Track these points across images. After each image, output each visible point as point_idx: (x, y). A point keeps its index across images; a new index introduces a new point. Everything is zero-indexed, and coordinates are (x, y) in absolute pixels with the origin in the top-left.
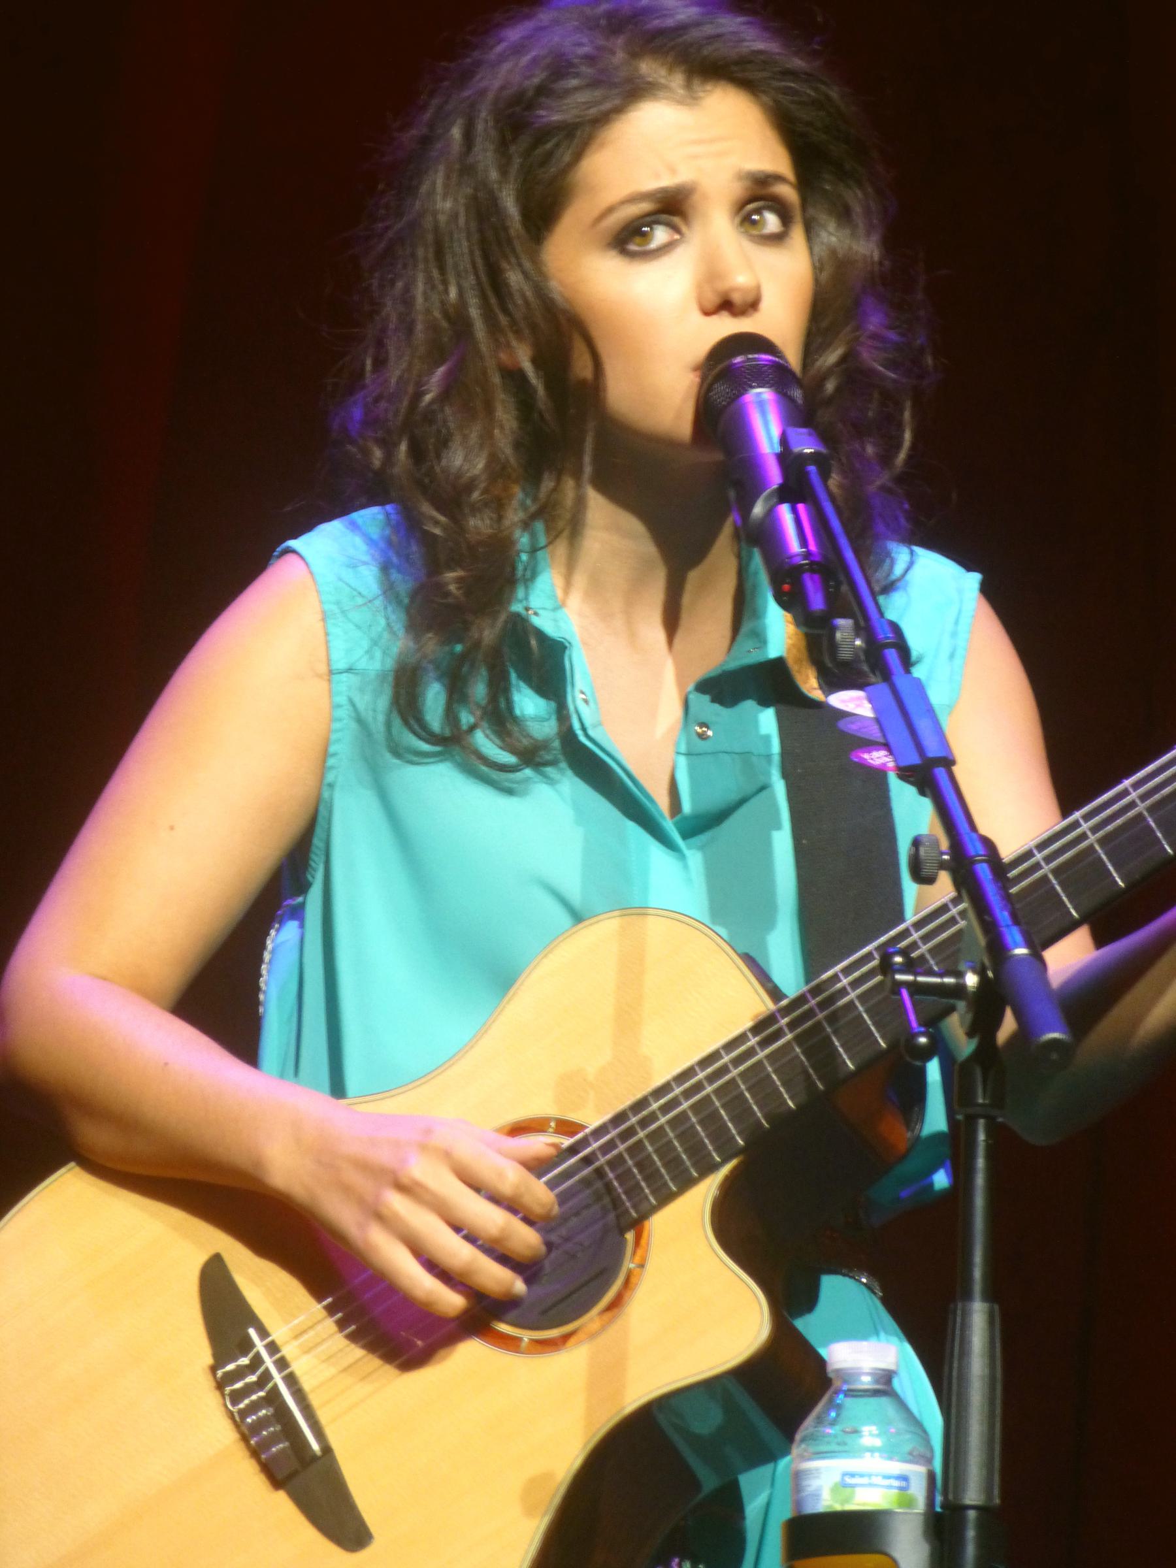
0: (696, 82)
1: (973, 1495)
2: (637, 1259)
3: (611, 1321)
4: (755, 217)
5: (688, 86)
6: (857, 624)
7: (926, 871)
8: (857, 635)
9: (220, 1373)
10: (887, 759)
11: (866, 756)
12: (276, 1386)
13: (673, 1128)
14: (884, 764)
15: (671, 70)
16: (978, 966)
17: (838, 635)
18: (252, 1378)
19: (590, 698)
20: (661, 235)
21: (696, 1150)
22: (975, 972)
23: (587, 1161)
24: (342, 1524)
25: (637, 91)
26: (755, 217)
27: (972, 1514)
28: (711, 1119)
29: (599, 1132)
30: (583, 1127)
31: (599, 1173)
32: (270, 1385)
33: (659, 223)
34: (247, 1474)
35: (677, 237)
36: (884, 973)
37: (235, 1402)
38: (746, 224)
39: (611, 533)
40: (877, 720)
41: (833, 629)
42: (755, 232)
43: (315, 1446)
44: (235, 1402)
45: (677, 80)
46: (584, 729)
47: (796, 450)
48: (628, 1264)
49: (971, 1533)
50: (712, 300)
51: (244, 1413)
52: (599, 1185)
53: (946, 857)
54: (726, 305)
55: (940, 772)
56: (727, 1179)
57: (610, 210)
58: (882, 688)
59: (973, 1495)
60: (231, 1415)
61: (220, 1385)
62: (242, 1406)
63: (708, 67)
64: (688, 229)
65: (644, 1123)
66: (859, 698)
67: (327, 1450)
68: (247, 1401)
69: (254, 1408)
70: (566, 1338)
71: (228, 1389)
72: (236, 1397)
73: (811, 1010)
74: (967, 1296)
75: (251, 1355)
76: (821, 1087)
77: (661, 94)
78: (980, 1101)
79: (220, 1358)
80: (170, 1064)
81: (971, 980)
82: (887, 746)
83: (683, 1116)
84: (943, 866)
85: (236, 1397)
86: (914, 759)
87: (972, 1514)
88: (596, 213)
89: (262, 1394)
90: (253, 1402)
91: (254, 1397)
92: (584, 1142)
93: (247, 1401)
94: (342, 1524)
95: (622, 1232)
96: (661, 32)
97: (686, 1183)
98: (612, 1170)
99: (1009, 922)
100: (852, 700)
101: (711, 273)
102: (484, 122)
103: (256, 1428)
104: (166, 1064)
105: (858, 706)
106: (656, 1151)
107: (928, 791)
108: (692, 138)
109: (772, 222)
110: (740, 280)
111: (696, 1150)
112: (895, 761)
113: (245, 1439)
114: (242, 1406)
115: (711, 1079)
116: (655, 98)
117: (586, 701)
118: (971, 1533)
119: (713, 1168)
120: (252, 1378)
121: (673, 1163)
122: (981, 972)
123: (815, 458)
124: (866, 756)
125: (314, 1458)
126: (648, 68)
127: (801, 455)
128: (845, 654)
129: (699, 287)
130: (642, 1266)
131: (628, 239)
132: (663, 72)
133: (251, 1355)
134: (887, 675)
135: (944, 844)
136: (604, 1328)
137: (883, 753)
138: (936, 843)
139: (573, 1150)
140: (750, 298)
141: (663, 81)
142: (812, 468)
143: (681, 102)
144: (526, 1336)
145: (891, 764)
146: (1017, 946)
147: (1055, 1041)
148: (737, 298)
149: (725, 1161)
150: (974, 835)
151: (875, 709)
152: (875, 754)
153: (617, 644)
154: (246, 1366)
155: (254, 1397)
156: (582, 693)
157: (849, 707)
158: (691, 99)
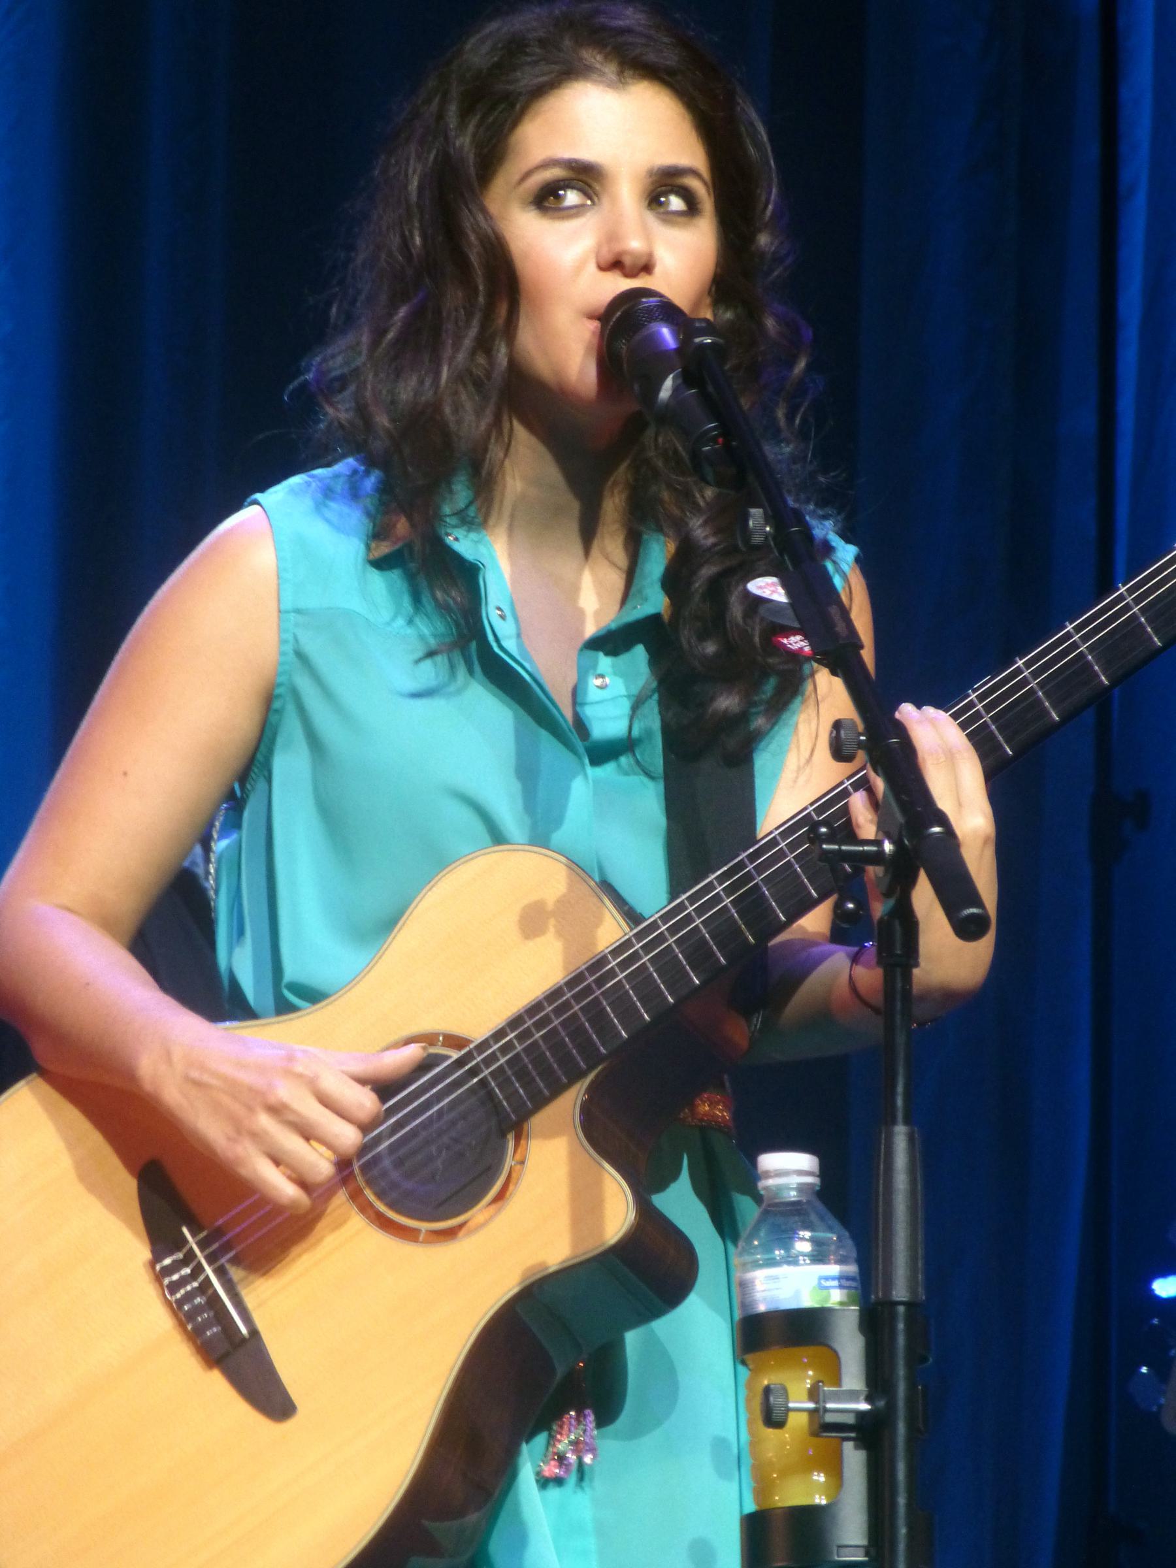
1: (900, 1293)
2: (518, 1157)
3: (499, 1211)
4: (663, 199)
5: (620, 73)
6: (765, 513)
7: (846, 752)
8: (767, 523)
9: (158, 1267)
10: (803, 644)
11: (785, 641)
12: (207, 1277)
13: (494, 1079)
14: (801, 649)
15: (606, 57)
16: (896, 837)
17: (751, 523)
18: (187, 1271)
20: (572, 198)
21: (566, 1061)
22: (892, 841)
23: (473, 1072)
24: (268, 1396)
25: (570, 72)
26: (663, 199)
27: (901, 1309)
28: (577, 1032)
29: (483, 1046)
30: (468, 1042)
31: (483, 1083)
32: (202, 1278)
33: (573, 188)
34: (181, 1357)
35: (589, 202)
36: (812, 841)
37: (172, 1292)
38: (654, 206)
39: (526, 466)
41: (745, 517)
42: (662, 210)
43: (244, 1330)
44: (172, 1292)
45: (611, 69)
48: (509, 1162)
49: (901, 1326)
50: (607, 256)
51: (180, 1303)
52: (482, 1093)
53: (862, 738)
54: (616, 265)
56: (592, 1082)
59: (900, 1293)
60: (168, 1303)
61: (159, 1277)
62: (178, 1296)
63: (636, 65)
64: (610, 191)
65: (600, 982)
66: (773, 584)
67: (254, 1332)
68: (182, 1292)
69: (188, 1297)
70: (461, 1226)
71: (166, 1281)
72: (174, 1287)
73: (589, 987)
74: (894, 1122)
75: (185, 1250)
76: (671, 1000)
77: (595, 76)
79: (157, 1257)
80: (99, 978)
81: (888, 847)
83: (554, 1031)
84: (860, 745)
85: (174, 1287)
89: (195, 1284)
90: (187, 1293)
91: (189, 1288)
92: (469, 1056)
93: (182, 1292)
94: (268, 1396)
95: (503, 1135)
96: (604, 28)
97: (557, 1090)
98: (606, 999)
101: (612, 236)
102: (455, 91)
103: (191, 1316)
104: (88, 984)
106: (531, 1062)
107: (839, 672)
108: (616, 122)
109: (676, 203)
110: (635, 244)
111: (566, 1061)
113: (182, 1325)
114: (178, 1296)
115: (647, 948)
116: (595, 82)
117: (503, 617)
118: (901, 1326)
119: (582, 1075)
120: (187, 1271)
121: (547, 1073)
124: (785, 641)
125: (244, 1340)
126: (591, 56)
128: (757, 539)
129: (599, 246)
130: (522, 1163)
131: (546, 199)
132: (599, 58)
133: (185, 1250)
136: (491, 1218)
137: (798, 638)
139: (460, 1063)
141: (598, 66)
143: (611, 85)
144: (424, 1226)
148: (627, 260)
149: (591, 1068)
152: (793, 639)
153: (559, 591)
154: (181, 1261)
155: (189, 1288)
156: (499, 609)
157: (766, 593)
158: (620, 83)
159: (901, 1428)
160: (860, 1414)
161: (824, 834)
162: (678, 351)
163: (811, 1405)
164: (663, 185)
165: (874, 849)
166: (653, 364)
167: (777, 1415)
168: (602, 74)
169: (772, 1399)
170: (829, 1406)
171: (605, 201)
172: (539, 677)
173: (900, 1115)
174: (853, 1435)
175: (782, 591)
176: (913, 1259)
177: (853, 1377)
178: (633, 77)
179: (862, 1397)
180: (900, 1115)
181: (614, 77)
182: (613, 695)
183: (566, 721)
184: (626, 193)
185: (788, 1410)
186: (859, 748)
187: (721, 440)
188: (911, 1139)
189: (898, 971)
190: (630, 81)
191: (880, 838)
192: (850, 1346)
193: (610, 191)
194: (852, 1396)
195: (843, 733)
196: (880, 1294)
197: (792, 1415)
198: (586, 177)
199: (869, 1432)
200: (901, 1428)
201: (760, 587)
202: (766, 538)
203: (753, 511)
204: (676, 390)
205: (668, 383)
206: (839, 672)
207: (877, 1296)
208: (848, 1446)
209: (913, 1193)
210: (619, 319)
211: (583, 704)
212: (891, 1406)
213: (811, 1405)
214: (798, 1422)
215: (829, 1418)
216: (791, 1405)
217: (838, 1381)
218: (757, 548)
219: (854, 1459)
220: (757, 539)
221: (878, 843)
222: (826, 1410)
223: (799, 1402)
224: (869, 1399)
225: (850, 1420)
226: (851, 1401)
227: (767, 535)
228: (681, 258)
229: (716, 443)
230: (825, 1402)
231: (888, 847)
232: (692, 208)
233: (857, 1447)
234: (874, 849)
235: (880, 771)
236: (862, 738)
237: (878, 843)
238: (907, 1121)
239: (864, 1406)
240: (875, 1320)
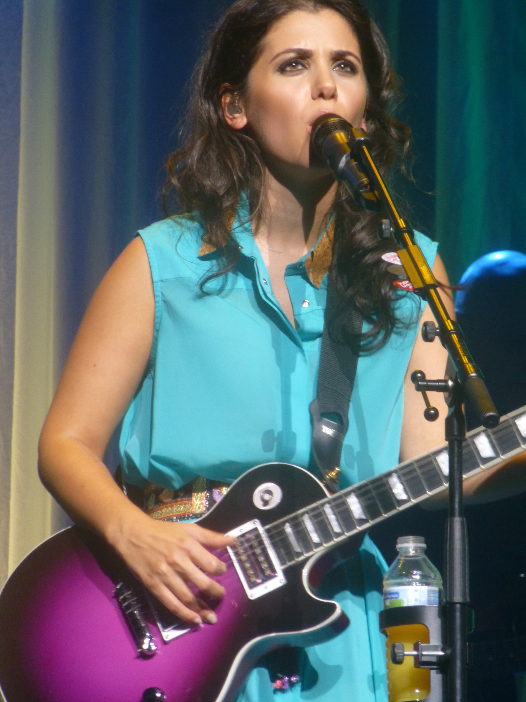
0: (319, 6)
1: (458, 598)
5: (315, 6)
6: (391, 221)
7: (430, 337)
8: (391, 226)
10: (409, 285)
11: (400, 284)
16: (454, 378)
19: (268, 281)
27: (458, 606)
39: (276, 196)
40: (403, 266)
41: (381, 224)
45: (310, 5)
46: (265, 294)
47: (357, 139)
49: (458, 614)
53: (438, 330)
54: (321, 95)
55: (432, 291)
57: (278, 55)
58: (404, 251)
59: (458, 598)
64: (311, 72)
66: (394, 256)
74: (453, 515)
78: (456, 434)
82: (408, 279)
84: (437, 334)
86: (421, 285)
87: (458, 606)
88: (272, 57)
99: (467, 362)
100: (392, 257)
105: (394, 260)
107: (426, 298)
108: (319, 32)
110: (328, 84)
112: (412, 285)
116: (302, 10)
117: (266, 283)
118: (458, 614)
122: (455, 381)
123: (365, 142)
124: (400, 284)
127: (360, 141)
128: (386, 234)
129: (312, 89)
131: (283, 68)
134: (406, 246)
135: (437, 325)
137: (407, 282)
138: (433, 324)
140: (331, 93)
142: (364, 147)
143: (311, 12)
145: (411, 287)
146: (472, 373)
147: (492, 416)
148: (326, 92)
150: (415, 247)
151: (401, 261)
152: (404, 283)
156: (264, 280)
157: (391, 261)
158: (315, 10)
159: (458, 663)
160: (439, 657)
161: (419, 377)
162: (348, 143)
163: (415, 653)
164: (339, 59)
165: (444, 384)
166: (336, 150)
167: (398, 659)
168: (307, 7)
169: (396, 650)
170: (424, 653)
171: (313, 67)
172: (281, 309)
173: (457, 512)
174: (435, 667)
175: (399, 259)
176: (464, 582)
177: (435, 639)
178: (321, 8)
179: (440, 649)
180: (457, 512)
181: (312, 8)
182: (312, 311)
183: (291, 325)
184: (322, 63)
185: (404, 655)
186: (436, 335)
187: (369, 186)
188: (462, 523)
189: (456, 443)
190: (319, 9)
191: (447, 378)
192: (433, 624)
193: (311, 72)
194: (435, 648)
195: (428, 328)
196: (448, 599)
197: (406, 657)
198: (302, 59)
199: (444, 665)
200: (458, 663)
201: (388, 258)
202: (391, 234)
203: (384, 221)
204: (347, 163)
205: (344, 159)
206: (426, 298)
207: (446, 600)
208: (433, 673)
209: (463, 550)
210: (320, 129)
211: (299, 315)
212: (454, 652)
213: (415, 653)
214: (409, 662)
215: (424, 659)
216: (406, 653)
217: (427, 641)
218: (386, 238)
219: (436, 678)
220: (386, 234)
221: (445, 381)
222: (422, 655)
223: (410, 651)
224: (443, 650)
225: (434, 660)
226: (434, 651)
227: (391, 232)
228: (349, 94)
229: (367, 188)
230: (422, 651)
231: (450, 383)
232: (353, 70)
233: (437, 673)
234: (444, 384)
235: (446, 346)
236: (438, 330)
237: (445, 381)
238: (460, 515)
239: (441, 653)
240: (446, 610)
